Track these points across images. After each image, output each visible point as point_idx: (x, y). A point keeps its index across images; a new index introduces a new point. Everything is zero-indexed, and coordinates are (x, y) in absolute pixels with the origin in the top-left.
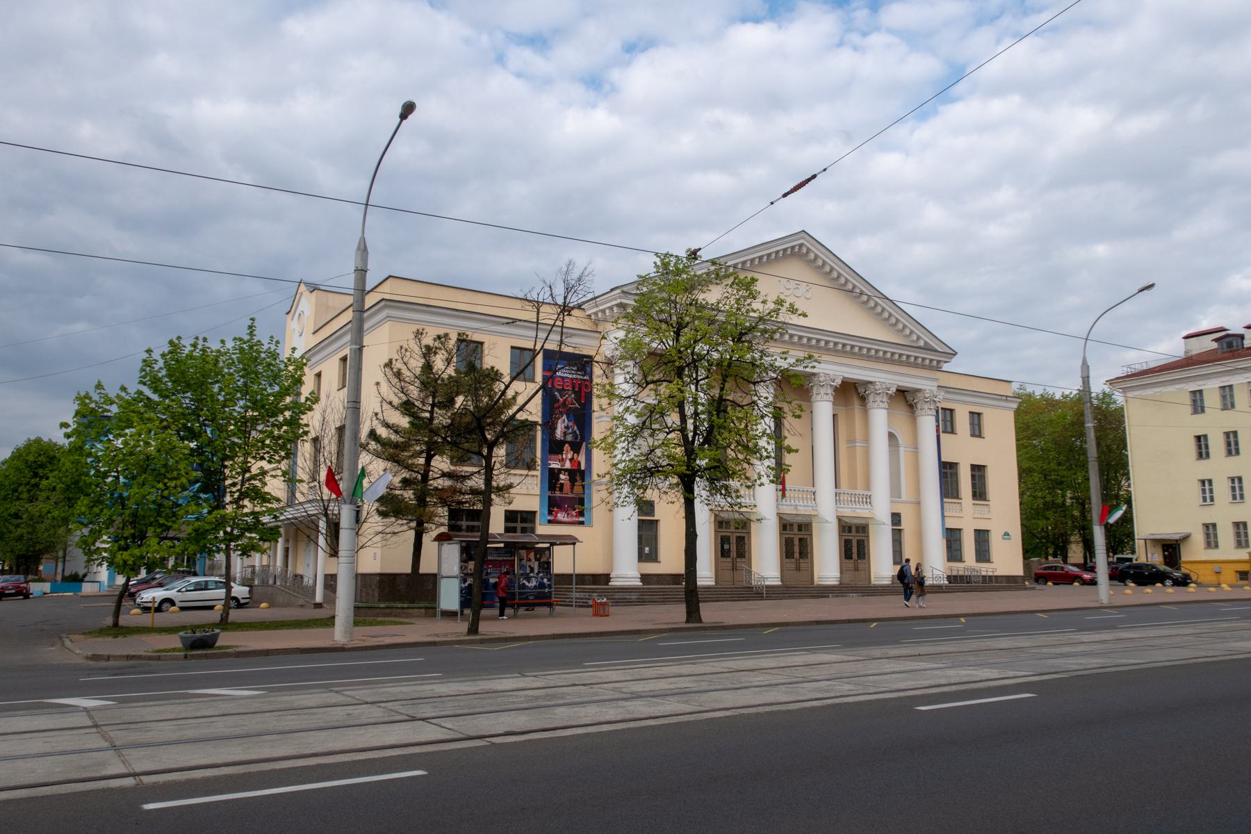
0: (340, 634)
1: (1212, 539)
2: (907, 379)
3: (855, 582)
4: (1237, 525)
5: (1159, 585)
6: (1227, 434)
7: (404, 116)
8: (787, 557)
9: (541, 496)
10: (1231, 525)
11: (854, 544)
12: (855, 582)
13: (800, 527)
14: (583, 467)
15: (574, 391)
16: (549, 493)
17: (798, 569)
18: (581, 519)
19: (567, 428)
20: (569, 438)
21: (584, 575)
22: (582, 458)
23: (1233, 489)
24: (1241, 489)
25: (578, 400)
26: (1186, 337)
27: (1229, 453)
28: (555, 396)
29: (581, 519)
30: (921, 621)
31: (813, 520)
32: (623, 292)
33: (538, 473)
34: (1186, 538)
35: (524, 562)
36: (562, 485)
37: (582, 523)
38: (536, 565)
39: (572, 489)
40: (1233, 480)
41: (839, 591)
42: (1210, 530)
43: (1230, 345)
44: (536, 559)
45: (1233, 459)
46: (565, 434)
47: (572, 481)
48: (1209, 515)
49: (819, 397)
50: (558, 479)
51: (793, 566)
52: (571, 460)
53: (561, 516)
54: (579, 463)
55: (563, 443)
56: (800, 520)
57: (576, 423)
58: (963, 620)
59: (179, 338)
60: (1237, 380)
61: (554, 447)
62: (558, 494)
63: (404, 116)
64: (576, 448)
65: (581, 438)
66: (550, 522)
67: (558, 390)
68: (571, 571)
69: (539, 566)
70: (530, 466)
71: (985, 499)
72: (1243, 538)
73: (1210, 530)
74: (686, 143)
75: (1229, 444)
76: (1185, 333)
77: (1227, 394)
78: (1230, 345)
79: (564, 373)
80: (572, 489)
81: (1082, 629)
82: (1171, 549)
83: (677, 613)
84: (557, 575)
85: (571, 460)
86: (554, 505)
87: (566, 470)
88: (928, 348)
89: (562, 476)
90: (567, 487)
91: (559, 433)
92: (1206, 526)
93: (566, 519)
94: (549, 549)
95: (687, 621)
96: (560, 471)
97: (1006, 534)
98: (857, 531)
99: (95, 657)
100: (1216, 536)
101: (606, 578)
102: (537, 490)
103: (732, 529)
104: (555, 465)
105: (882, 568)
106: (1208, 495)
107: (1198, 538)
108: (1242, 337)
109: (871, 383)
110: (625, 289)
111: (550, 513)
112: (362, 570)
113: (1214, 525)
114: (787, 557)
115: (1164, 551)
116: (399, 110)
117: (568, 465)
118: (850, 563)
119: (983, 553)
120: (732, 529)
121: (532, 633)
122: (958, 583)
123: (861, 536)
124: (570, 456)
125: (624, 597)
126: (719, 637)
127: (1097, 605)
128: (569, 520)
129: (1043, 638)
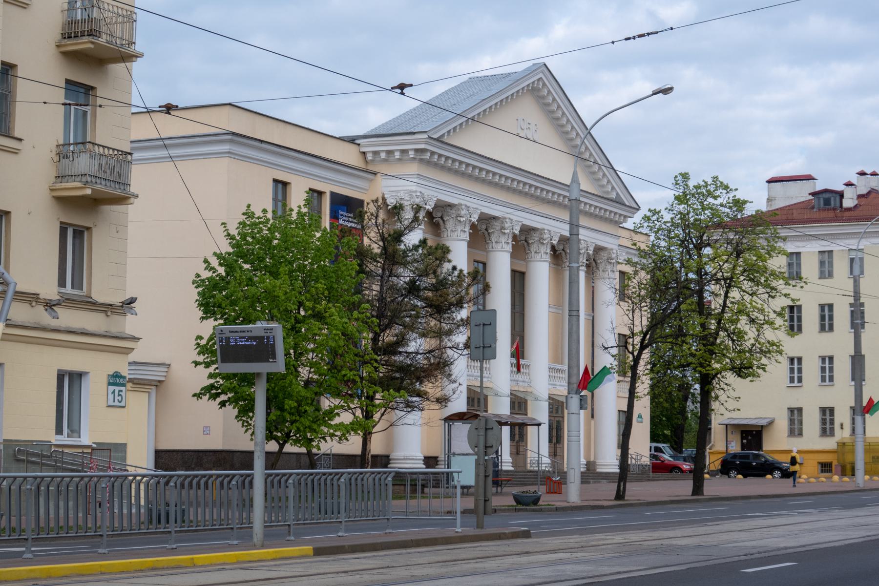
0: (861, 478)
1: (828, 426)
4: (823, 410)
5: (769, 476)
6: (822, 307)
10: (818, 410)
21: (125, 452)
23: (823, 369)
24: (831, 369)
26: (769, 182)
27: (822, 329)
32: (430, 138)
34: (771, 423)
40: (823, 359)
42: (795, 414)
43: (827, 202)
45: (826, 335)
48: (795, 398)
49: (499, 246)
59: (249, 206)
60: (836, 247)
72: (828, 426)
73: (795, 414)
75: (823, 318)
76: (768, 178)
77: (826, 261)
78: (827, 202)
82: (752, 436)
83: (685, 487)
88: (618, 202)
92: (791, 410)
95: (694, 494)
99: (176, 522)
100: (801, 422)
106: (796, 375)
107: (782, 424)
108: (841, 195)
109: (495, 218)
113: (800, 410)
115: (742, 438)
126: (798, 500)
127: (565, 504)
129: (650, 534)
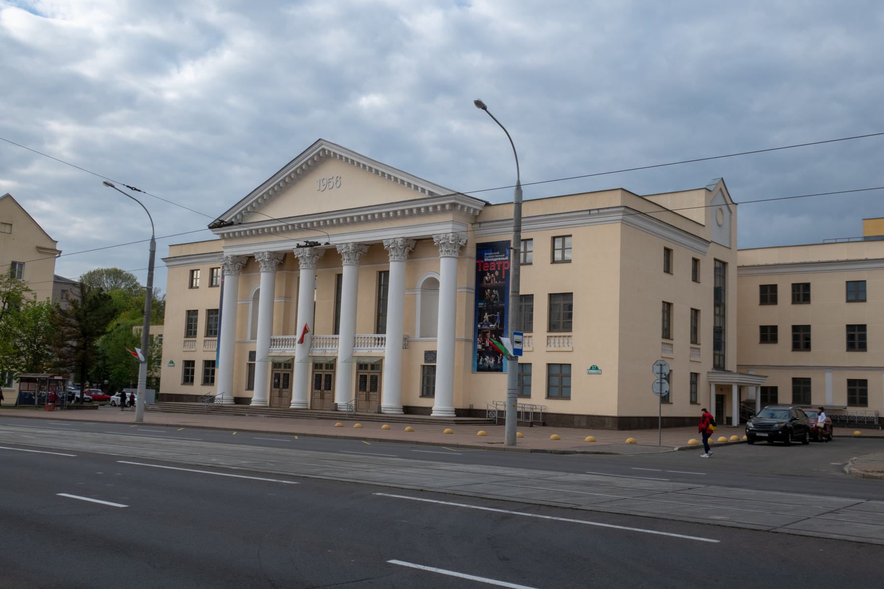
2: (419, 229)
3: (278, 407)
8: (360, 390)
11: (323, 378)
12: (278, 407)
13: (373, 367)
30: (270, 435)
41: (351, 417)
56: (373, 361)
58: (296, 437)
63: (484, 108)
68: (658, 415)
81: (84, 430)
84: (163, 394)
97: (172, 362)
98: (285, 367)
103: (324, 369)
105: (388, 400)
114: (360, 390)
119: (209, 379)
120: (282, 369)
121: (270, 430)
123: (329, 372)
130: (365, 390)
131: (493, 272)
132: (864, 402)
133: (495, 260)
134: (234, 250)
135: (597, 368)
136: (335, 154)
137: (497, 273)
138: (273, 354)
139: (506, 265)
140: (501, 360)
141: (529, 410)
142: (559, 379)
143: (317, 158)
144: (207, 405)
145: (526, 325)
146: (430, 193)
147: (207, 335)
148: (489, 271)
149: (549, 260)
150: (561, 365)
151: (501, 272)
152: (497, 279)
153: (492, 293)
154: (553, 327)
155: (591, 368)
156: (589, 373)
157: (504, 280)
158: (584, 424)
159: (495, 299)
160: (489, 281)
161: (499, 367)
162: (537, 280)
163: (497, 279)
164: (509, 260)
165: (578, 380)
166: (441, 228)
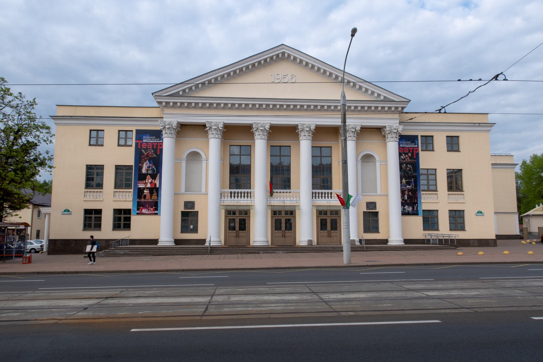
7: (353, 35)
8: (276, 229)
9: (133, 201)
14: (157, 186)
15: (153, 149)
16: (137, 200)
17: (284, 236)
18: (156, 212)
19: (149, 167)
20: (150, 172)
22: (157, 182)
25: (156, 154)
28: (142, 152)
29: (156, 212)
31: (297, 208)
33: (132, 190)
35: (10, 236)
36: (145, 195)
37: (157, 214)
38: (17, 238)
39: (151, 197)
41: (309, 249)
44: (17, 234)
46: (147, 170)
47: (151, 193)
50: (143, 192)
51: (281, 235)
52: (151, 183)
53: (144, 211)
54: (155, 184)
55: (146, 175)
56: (287, 209)
57: (154, 164)
61: (142, 177)
62: (143, 200)
63: (353, 35)
64: (154, 177)
65: (156, 172)
66: (138, 214)
67: (144, 149)
69: (19, 238)
70: (128, 186)
71: (462, 191)
74: (518, 22)
79: (146, 139)
80: (151, 197)
85: (151, 183)
86: (140, 205)
87: (147, 188)
89: (145, 191)
90: (148, 196)
91: (144, 171)
93: (147, 212)
94: (25, 229)
96: (144, 189)
97: (480, 213)
101: (156, 241)
102: (131, 198)
104: (141, 186)
110: (157, 94)
111: (138, 209)
112: (50, 238)
114: (276, 229)
116: (350, 33)
117: (149, 185)
118: (279, 233)
122: (410, 244)
124: (150, 181)
125: (165, 252)
126: (185, 276)
128: (149, 212)
130: (280, 229)
131: (407, 154)
132: (462, 228)
133: (408, 146)
134: (366, 121)
135: (481, 213)
136: (289, 56)
137: (410, 154)
138: (225, 204)
139: (416, 150)
140: (417, 208)
141: (441, 238)
142: (457, 219)
143: (280, 56)
144: (149, 246)
145: (433, 189)
146: (385, 97)
147: (117, 186)
148: (404, 153)
149: (88, 143)
150: (455, 211)
151: (412, 154)
152: (410, 158)
153: (407, 167)
154: (450, 188)
155: (478, 213)
156: (477, 215)
157: (415, 159)
158: (476, 244)
159: (410, 170)
160: (405, 159)
161: (415, 212)
162: (435, 161)
163: (410, 158)
164: (418, 147)
165: (469, 219)
166: (390, 122)
